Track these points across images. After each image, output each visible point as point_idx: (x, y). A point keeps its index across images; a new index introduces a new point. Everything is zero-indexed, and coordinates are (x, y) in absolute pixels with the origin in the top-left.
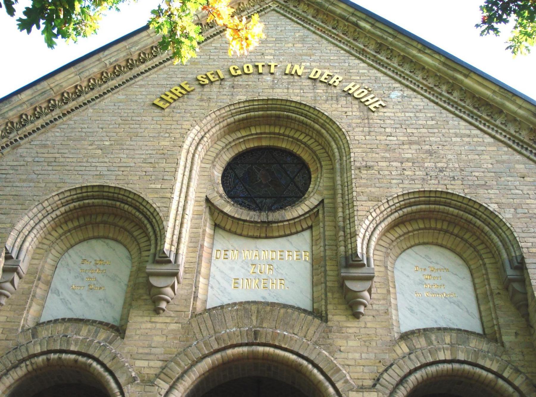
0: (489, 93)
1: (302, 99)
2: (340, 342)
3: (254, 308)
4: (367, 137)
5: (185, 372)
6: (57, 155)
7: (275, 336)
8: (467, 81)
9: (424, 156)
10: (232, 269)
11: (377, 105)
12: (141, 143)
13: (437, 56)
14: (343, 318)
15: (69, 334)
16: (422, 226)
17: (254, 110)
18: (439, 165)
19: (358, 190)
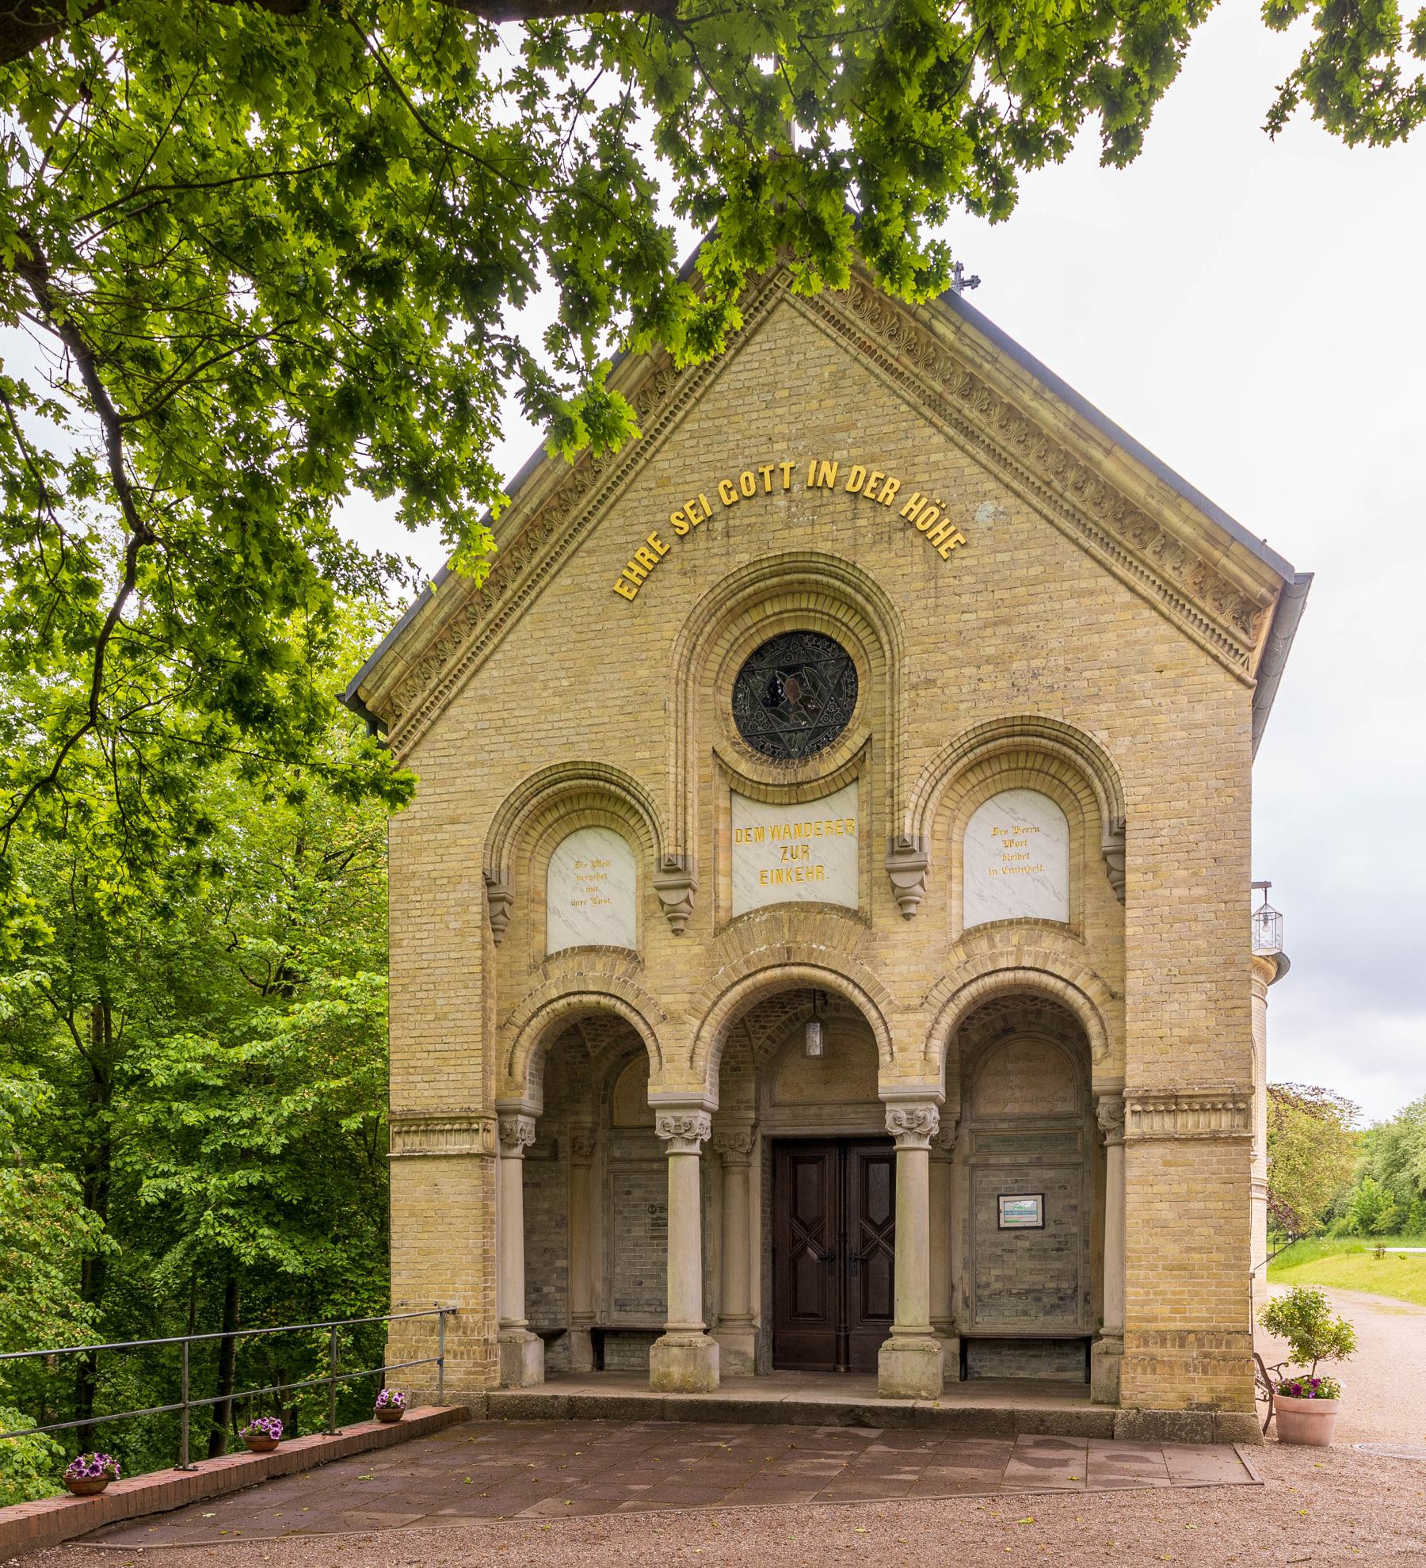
0: (1139, 490)
1: (838, 546)
2: (885, 954)
5: (715, 1004)
6: (505, 714)
7: (811, 951)
8: (1109, 465)
9: (1012, 648)
11: (951, 544)
12: (612, 677)
13: (1062, 407)
14: (891, 921)
15: (583, 969)
16: (1005, 767)
17: (765, 578)
18: (1035, 663)
19: (911, 728)
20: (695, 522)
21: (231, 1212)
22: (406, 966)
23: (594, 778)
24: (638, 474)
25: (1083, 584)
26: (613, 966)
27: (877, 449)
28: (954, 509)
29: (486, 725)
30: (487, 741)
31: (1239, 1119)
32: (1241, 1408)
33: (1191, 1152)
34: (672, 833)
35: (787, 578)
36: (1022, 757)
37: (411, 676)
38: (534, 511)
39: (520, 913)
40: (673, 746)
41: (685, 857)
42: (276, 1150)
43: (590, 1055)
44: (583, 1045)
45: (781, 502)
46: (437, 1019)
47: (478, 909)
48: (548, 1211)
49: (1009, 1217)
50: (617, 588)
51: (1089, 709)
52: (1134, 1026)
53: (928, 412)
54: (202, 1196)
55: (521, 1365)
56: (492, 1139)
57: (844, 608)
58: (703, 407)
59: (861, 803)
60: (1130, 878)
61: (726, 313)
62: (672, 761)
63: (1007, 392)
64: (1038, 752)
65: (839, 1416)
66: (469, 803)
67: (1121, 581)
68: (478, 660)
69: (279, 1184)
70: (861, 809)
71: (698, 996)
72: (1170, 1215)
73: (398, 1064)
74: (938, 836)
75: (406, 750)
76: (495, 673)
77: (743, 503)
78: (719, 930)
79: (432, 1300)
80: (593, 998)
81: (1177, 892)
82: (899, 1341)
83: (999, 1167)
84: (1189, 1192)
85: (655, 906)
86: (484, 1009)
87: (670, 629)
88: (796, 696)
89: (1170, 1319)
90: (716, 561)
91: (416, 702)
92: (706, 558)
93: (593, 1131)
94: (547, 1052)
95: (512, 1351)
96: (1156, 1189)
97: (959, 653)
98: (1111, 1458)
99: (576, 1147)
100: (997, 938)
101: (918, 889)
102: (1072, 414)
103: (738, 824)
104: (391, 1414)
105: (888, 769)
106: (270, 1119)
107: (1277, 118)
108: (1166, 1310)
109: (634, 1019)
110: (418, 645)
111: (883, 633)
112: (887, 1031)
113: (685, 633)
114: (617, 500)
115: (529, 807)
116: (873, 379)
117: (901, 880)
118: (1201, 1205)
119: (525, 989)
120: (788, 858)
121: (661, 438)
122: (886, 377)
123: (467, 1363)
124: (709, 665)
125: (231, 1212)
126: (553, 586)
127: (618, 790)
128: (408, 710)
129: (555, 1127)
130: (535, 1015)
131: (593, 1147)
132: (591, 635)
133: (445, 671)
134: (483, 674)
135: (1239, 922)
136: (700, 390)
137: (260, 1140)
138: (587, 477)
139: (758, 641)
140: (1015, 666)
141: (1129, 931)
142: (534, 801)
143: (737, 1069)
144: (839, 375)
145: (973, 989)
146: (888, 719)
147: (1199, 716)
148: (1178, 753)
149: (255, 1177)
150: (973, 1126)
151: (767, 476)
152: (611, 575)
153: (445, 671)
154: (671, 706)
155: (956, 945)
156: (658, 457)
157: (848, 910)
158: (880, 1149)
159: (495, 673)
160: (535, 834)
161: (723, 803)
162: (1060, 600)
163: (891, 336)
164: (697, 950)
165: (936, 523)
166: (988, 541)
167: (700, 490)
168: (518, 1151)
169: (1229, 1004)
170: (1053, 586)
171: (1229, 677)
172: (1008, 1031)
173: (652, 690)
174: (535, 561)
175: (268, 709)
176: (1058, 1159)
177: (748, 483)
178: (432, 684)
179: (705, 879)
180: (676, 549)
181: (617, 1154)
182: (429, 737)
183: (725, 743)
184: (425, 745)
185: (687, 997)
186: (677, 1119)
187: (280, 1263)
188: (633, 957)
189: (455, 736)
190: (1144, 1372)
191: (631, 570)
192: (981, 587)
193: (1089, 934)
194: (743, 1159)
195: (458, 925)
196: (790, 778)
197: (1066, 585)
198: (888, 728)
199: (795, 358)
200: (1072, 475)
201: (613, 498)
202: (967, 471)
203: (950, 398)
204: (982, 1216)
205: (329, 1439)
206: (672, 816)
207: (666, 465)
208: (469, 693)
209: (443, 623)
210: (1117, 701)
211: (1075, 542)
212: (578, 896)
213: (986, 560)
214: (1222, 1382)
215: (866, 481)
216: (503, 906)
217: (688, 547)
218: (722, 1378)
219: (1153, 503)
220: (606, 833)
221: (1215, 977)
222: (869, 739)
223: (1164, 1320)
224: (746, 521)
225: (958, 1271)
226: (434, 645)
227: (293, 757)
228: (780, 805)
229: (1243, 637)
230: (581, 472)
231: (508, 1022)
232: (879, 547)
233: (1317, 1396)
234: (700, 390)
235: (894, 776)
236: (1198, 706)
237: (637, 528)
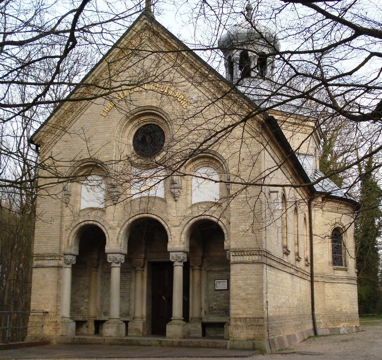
5: (124, 224)
14: (172, 202)
33: (247, 266)
43: (91, 238)
84: (247, 278)
87: (115, 124)
89: (242, 314)
96: (238, 277)
118: (250, 282)
130: (75, 227)
158: (170, 266)
186: (113, 257)
190: (235, 330)
191: (106, 109)
204: (210, 286)
209: (56, 122)
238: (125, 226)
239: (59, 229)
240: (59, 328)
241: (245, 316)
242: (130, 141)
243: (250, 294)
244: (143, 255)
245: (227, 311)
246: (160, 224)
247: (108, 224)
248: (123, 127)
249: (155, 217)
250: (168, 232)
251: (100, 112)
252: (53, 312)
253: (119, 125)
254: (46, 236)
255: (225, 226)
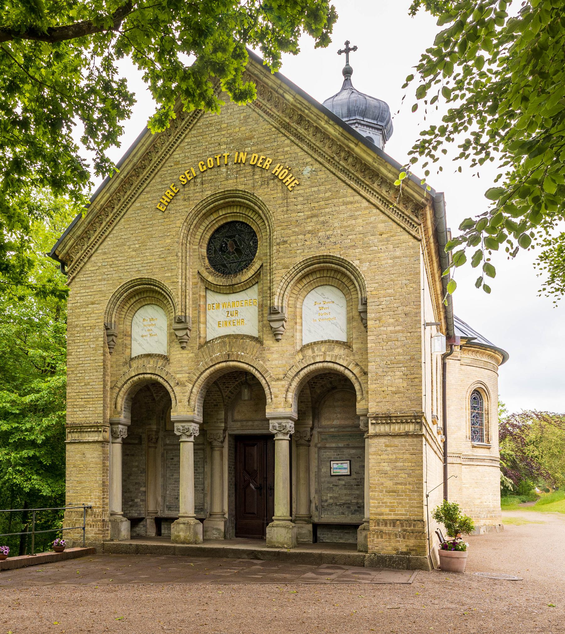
0: (370, 160)
1: (246, 187)
2: (269, 356)
3: (227, 340)
4: (286, 216)
5: (198, 378)
6: (113, 259)
7: (238, 355)
9: (319, 227)
10: (217, 316)
11: (293, 184)
12: (155, 243)
14: (271, 342)
16: (318, 276)
17: (218, 200)
18: (328, 233)
19: (277, 261)
20: (189, 179)
21: (21, 468)
22: (73, 363)
23: (149, 284)
24: (166, 160)
25: (348, 199)
26: (157, 362)
27: (262, 147)
28: (294, 170)
29: (106, 264)
30: (106, 270)
31: (417, 427)
32: (420, 554)
33: (397, 441)
34: (180, 306)
35: (227, 200)
36: (325, 272)
37: (77, 245)
38: (125, 177)
39: (120, 341)
40: (180, 271)
41: (185, 317)
42: (39, 442)
43: (149, 399)
44: (152, 395)
45: (224, 170)
46: (85, 385)
47: (102, 339)
48: (137, 466)
49: (335, 471)
50: (158, 207)
51: (351, 251)
52: (372, 386)
53: (283, 131)
54: (9, 461)
55: (119, 531)
56: (108, 435)
57: (251, 212)
58: (193, 132)
59: (259, 292)
60: (369, 323)
61: (169, 113)
62: (180, 277)
63: (315, 121)
64: (332, 269)
65: (248, 555)
66: (99, 296)
67: (364, 198)
68: (103, 238)
69: (43, 456)
70: (259, 295)
71: (192, 375)
72: (388, 469)
73: (69, 404)
74: (290, 306)
75: (74, 275)
76: (110, 243)
77: (209, 170)
78: (201, 346)
79: (82, 503)
80: (149, 376)
81: (390, 329)
82: (276, 522)
83: (331, 448)
84: (396, 458)
85: (174, 337)
86: (104, 381)
88: (233, 248)
89: (389, 514)
90: (198, 194)
91: (79, 255)
92: (194, 194)
93: (157, 432)
94: (132, 398)
95: (115, 524)
97: (296, 230)
98: (353, 573)
99: (149, 439)
100: (316, 349)
101: (282, 328)
102: (341, 130)
103: (209, 302)
104: (60, 548)
105: (268, 278)
106: (38, 428)
107: (414, 10)
108: (387, 510)
109: (165, 384)
110: (79, 232)
111: (266, 222)
112: (270, 389)
113: (185, 224)
114: (158, 171)
115: (123, 297)
116: (261, 118)
117: (275, 325)
119: (121, 372)
120: (229, 315)
121: (176, 145)
122: (266, 117)
123: (95, 529)
124: (196, 237)
125: (21, 468)
126: (133, 206)
127: (159, 289)
128: (75, 258)
129: (141, 430)
130: (126, 383)
131: (157, 439)
132: (148, 226)
133: (90, 242)
134: (105, 243)
135: (416, 341)
136: (192, 126)
137: (33, 437)
138: (146, 162)
139: (217, 226)
140: (320, 234)
141: (369, 345)
142: (125, 294)
143: (217, 405)
144: (247, 117)
145: (305, 371)
146: (268, 257)
147: (398, 253)
148: (389, 269)
149: (31, 453)
150: (319, 430)
151: (218, 159)
152: (155, 201)
153: (90, 242)
154: (180, 254)
155: (298, 352)
156: (175, 153)
157: (254, 337)
158: (268, 440)
159: (110, 243)
160: (126, 308)
161: (203, 293)
162: (339, 206)
163: (268, 100)
164: (191, 355)
165: (287, 176)
166: (308, 183)
167: (191, 166)
168: (119, 440)
169: (412, 376)
170: (335, 201)
171: (410, 237)
172: (334, 388)
173: (172, 248)
174: (126, 197)
175: (7, 266)
176: (357, 445)
177: (210, 163)
178: (85, 248)
179: (194, 325)
180: (182, 190)
181: (168, 442)
182: (84, 269)
183: (203, 269)
184: (82, 272)
185: (187, 375)
186: (183, 427)
187: (40, 491)
188: (166, 358)
189: (94, 268)
190: (378, 538)
191: (163, 199)
192: (306, 202)
193: (354, 346)
194: (220, 444)
195: (94, 346)
196: (229, 283)
197: (341, 200)
198: (269, 261)
199: (229, 111)
200: (343, 154)
201: (157, 170)
202: (299, 154)
203: (292, 124)
205: (31, 557)
206: (180, 300)
207: (178, 156)
208: (99, 251)
209: (89, 223)
210: (363, 248)
211: (344, 182)
212: (144, 333)
213: (308, 190)
214: (412, 542)
215: (258, 160)
216: (113, 338)
217: (186, 189)
218: (204, 539)
219: (376, 165)
220: (155, 307)
221: (406, 365)
222: (262, 266)
223: (386, 515)
224: (210, 178)
225: (313, 494)
226: (86, 232)
227: (19, 282)
228: (226, 294)
229: (416, 219)
230: (144, 160)
231: (115, 386)
232: (264, 187)
233: (456, 550)
234: (192, 126)
235: (271, 281)
236: (397, 249)
237: (166, 182)
238: (200, 381)
239: (102, 386)
240: (108, 530)
241: (392, 517)
242: (203, 250)
243: (401, 484)
244: (223, 425)
245: (360, 508)
246: (254, 377)
247: (174, 378)
248: (192, 227)
249: (245, 366)
250: (267, 391)
251: (156, 204)
252: (99, 507)
253: (185, 224)
254: (83, 397)
255: (357, 378)
